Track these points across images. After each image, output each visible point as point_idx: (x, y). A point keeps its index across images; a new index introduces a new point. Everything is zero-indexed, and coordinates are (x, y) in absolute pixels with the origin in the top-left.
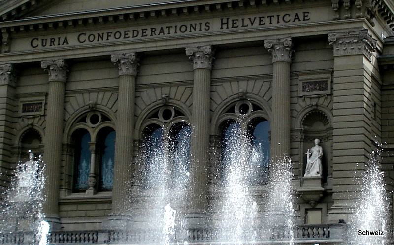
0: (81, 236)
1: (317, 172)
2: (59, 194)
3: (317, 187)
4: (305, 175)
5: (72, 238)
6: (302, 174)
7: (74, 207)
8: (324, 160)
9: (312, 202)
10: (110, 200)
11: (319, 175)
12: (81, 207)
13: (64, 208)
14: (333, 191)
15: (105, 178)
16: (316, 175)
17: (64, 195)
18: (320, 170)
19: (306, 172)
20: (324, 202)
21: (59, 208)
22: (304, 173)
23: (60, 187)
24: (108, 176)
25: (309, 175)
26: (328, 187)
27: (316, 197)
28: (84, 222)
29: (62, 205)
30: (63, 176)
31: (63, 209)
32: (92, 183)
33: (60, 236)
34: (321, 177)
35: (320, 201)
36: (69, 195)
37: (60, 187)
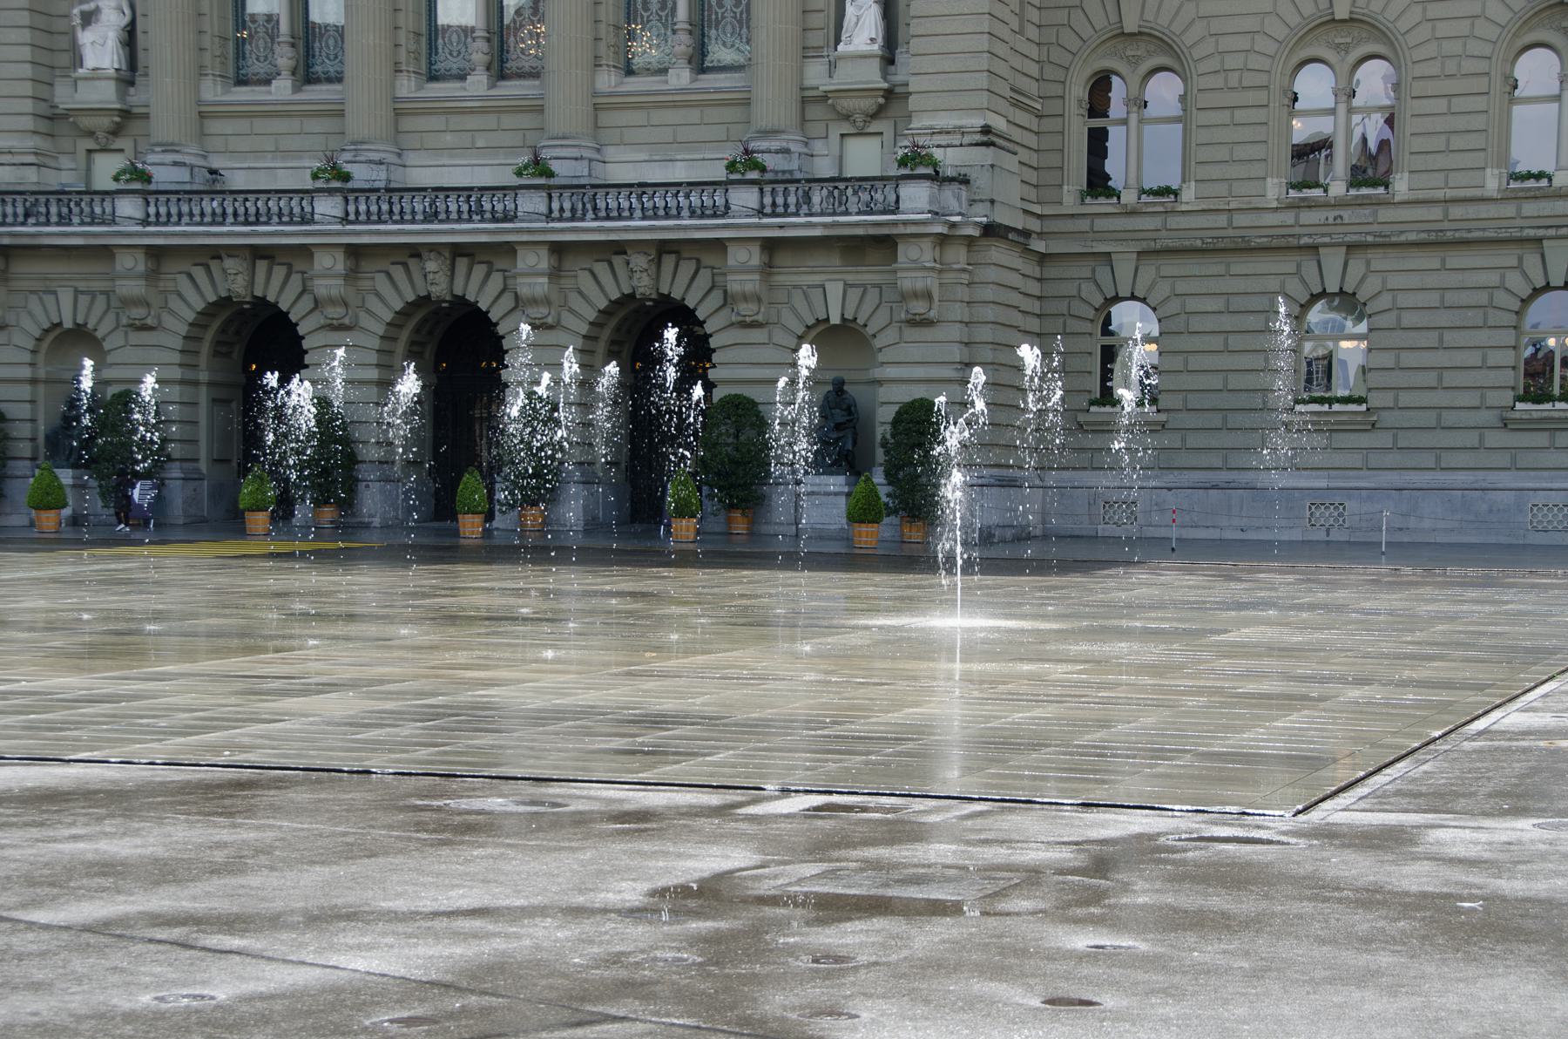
0: (271, 203)
1: (872, 39)
2: (393, 87)
3: (871, 75)
4: (840, 48)
5: (246, 209)
6: (832, 43)
7: (242, 125)
8: (130, 38)
9: (859, 118)
10: (540, 102)
11: (876, 47)
12: (260, 125)
13: (214, 126)
14: (911, 89)
15: (321, 48)
16: (869, 48)
17: (406, 87)
18: (877, 34)
19: (843, 38)
20: (887, 118)
21: (396, 123)
22: (838, 41)
23: (201, 72)
24: (450, 40)
25: (851, 48)
26: (899, 78)
27: (868, 104)
28: (272, 165)
29: (402, 114)
30: (402, 38)
31: (212, 131)
32: (683, 47)
33: (215, 204)
34: (880, 53)
35: (116, 132)
36: (223, 94)
37: (201, 72)
